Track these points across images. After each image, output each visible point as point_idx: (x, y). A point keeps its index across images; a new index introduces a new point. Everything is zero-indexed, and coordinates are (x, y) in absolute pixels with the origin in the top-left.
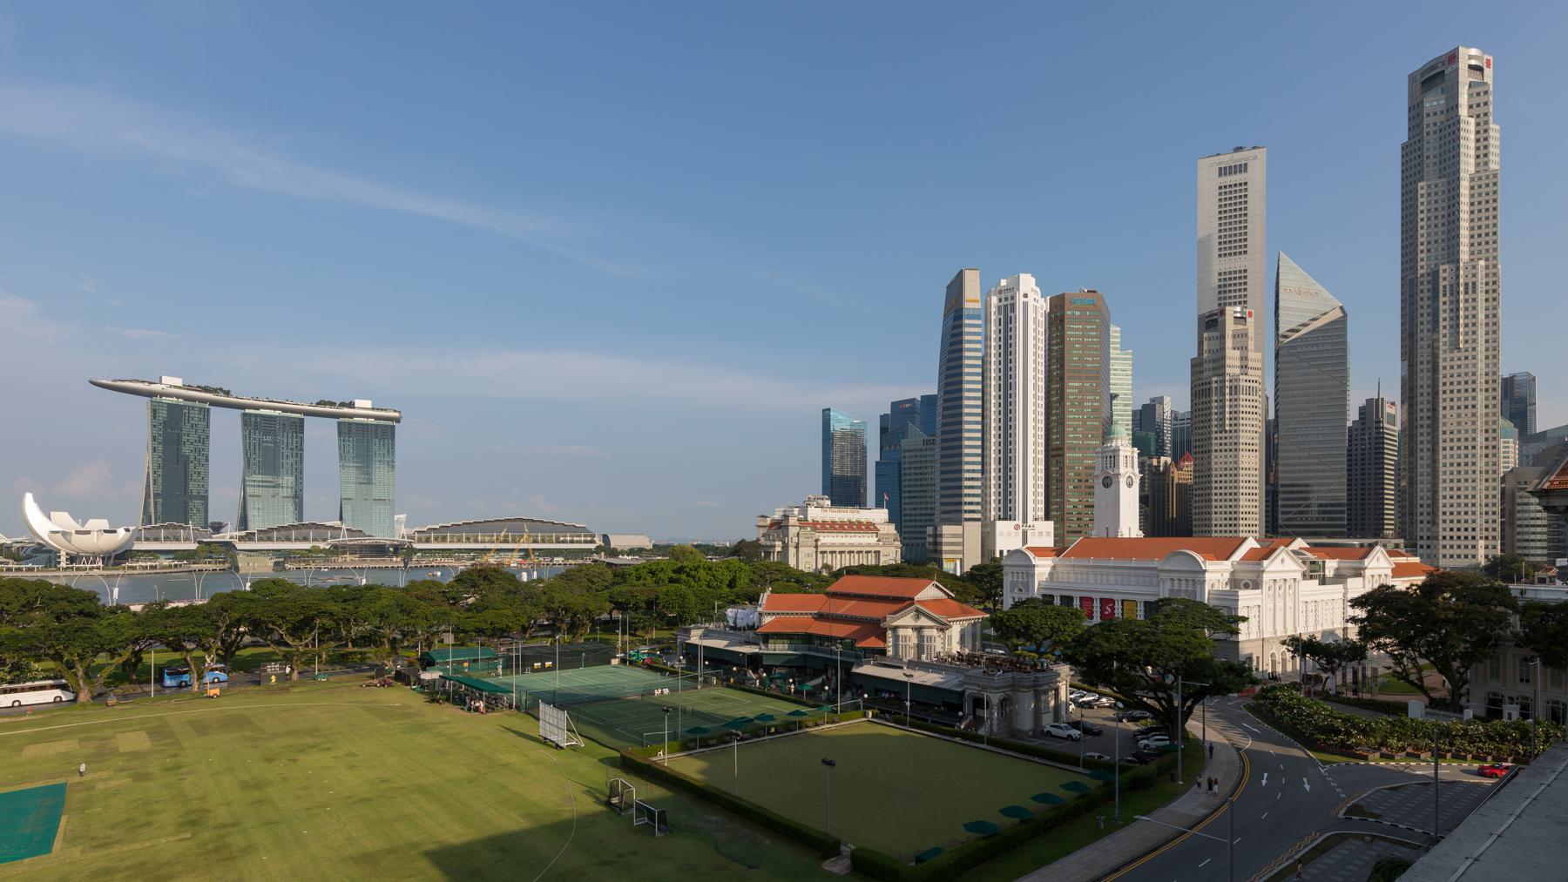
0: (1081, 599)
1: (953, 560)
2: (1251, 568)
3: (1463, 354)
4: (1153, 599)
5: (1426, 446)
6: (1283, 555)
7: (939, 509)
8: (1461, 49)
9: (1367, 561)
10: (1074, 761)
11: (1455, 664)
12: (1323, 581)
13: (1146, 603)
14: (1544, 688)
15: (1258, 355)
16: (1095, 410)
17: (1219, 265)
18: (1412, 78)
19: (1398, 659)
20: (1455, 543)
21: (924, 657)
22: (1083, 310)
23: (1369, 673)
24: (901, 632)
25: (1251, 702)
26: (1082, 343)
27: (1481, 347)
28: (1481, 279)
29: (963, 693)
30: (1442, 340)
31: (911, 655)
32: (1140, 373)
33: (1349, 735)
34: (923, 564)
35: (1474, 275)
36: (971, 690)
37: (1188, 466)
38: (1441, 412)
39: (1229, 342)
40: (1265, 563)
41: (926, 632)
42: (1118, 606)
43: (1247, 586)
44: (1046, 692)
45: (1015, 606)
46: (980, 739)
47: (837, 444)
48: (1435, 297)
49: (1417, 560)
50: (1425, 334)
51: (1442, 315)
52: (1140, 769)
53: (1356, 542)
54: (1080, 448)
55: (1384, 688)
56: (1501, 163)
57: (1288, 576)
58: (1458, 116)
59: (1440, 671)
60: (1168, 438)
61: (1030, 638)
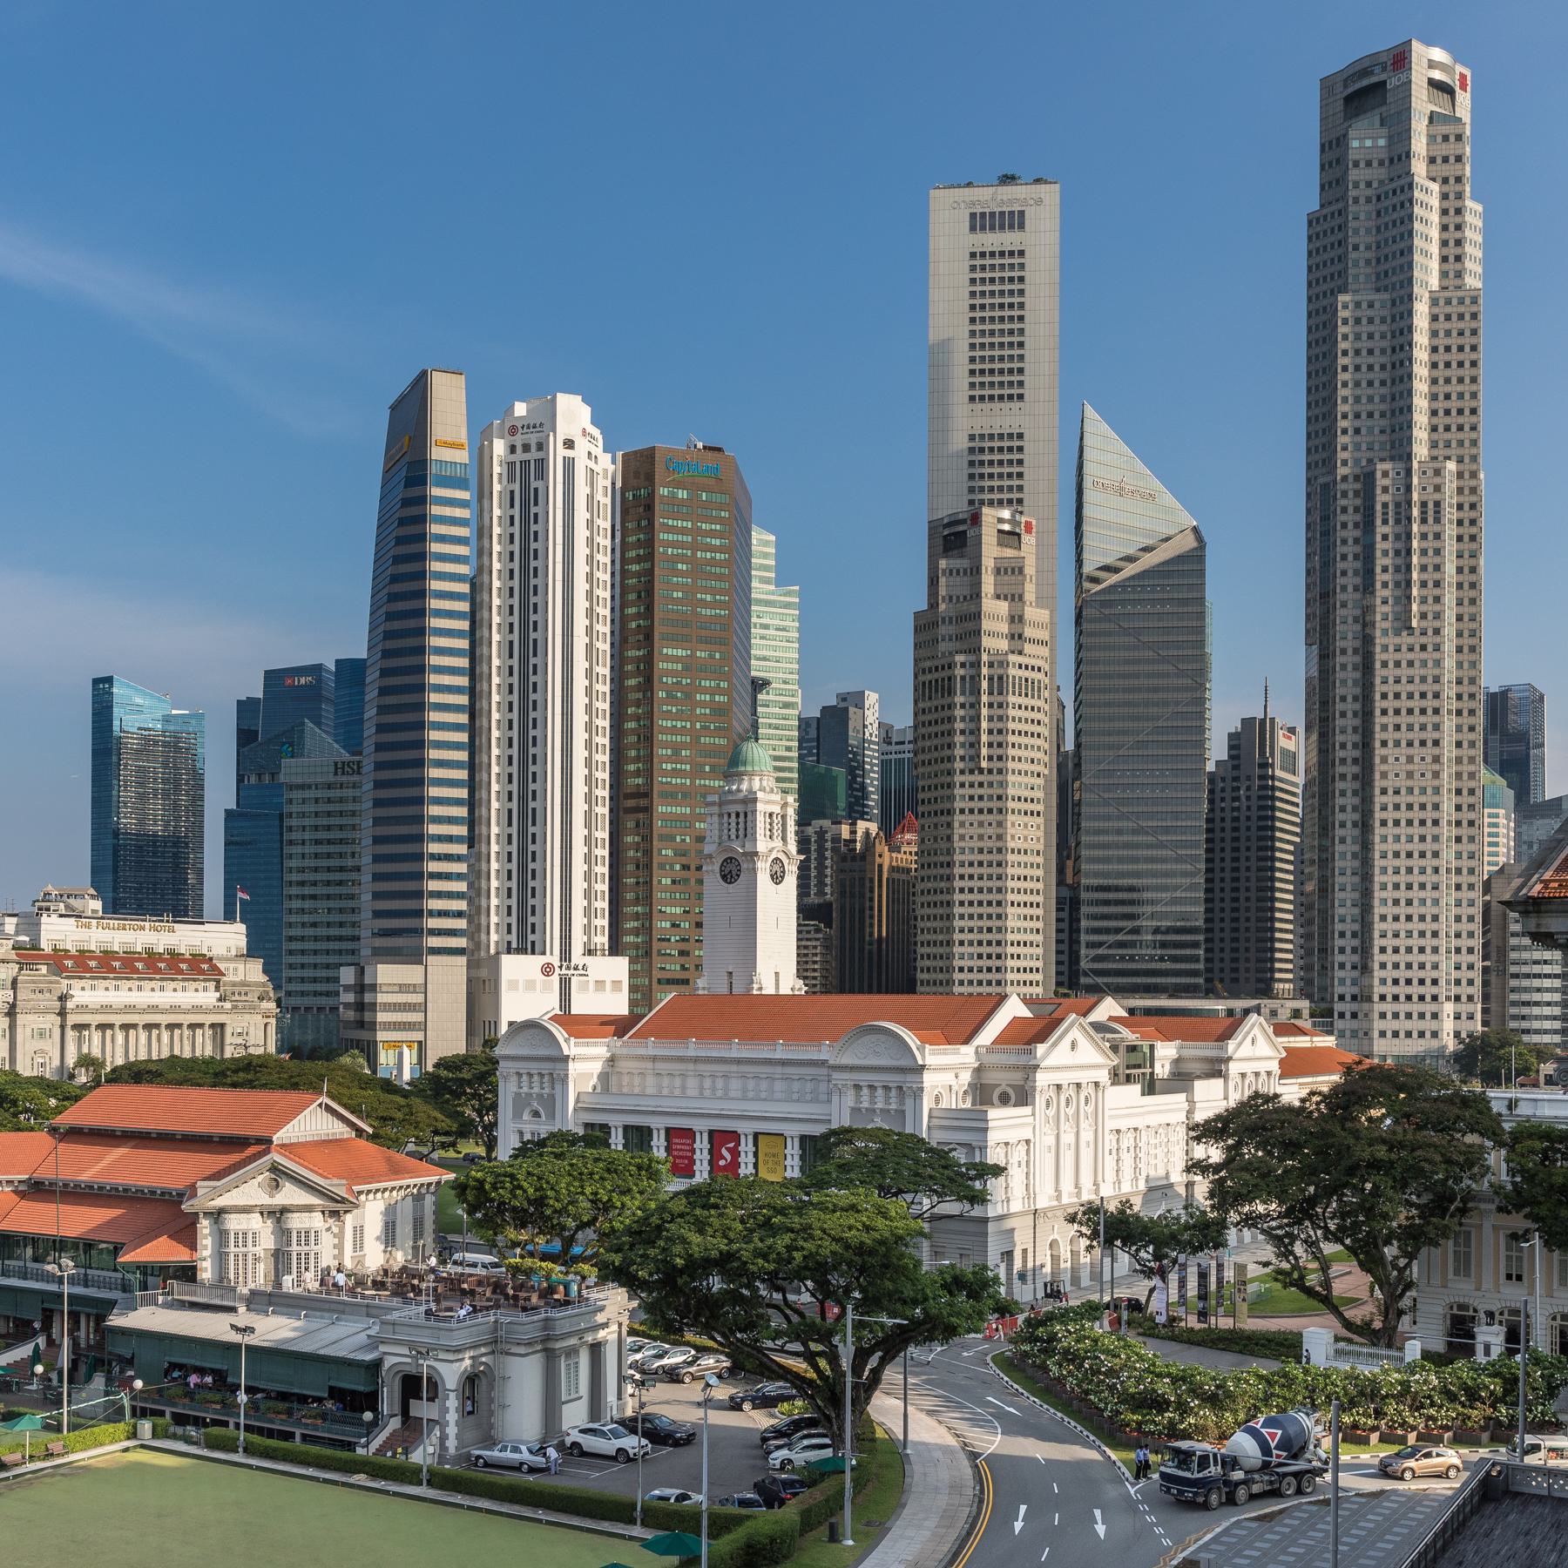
0: (670, 1132)
1: (396, 1045)
2: (1012, 1060)
3: (1417, 640)
4: (818, 1130)
5: (1350, 817)
6: (1075, 1033)
7: (368, 924)
8: (1416, 45)
9: (1231, 1045)
10: (621, 1511)
11: (1390, 1251)
12: (1151, 1088)
13: (803, 1139)
14: (1549, 1297)
15: (1043, 615)
16: (720, 711)
17: (967, 420)
18: (1327, 85)
19: (1283, 1244)
20: (1403, 1008)
21: (288, 1281)
22: (694, 488)
23: (1229, 1274)
24: (234, 1223)
25: (1008, 1349)
26: (691, 561)
27: (1449, 631)
28: (1450, 497)
29: (376, 1365)
30: (1381, 609)
31: (259, 1278)
32: (802, 639)
33: (1183, 1409)
34: (331, 1055)
35: (1438, 488)
36: (395, 1358)
37: (909, 841)
38: (1379, 751)
39: (988, 584)
40: (1041, 1049)
41: (296, 1222)
42: (746, 1147)
43: (1005, 1100)
44: (572, 1352)
45: (522, 1152)
46: (410, 1475)
47: (129, 768)
48: (1368, 525)
49: (1329, 1041)
50: (1350, 596)
51: (1381, 561)
52: (766, 1521)
53: (1220, 1006)
54: (686, 795)
55: (1260, 1305)
56: (1486, 277)
57: (1084, 1077)
58: (1409, 174)
59: (1363, 1266)
60: (873, 781)
61: (548, 1226)
